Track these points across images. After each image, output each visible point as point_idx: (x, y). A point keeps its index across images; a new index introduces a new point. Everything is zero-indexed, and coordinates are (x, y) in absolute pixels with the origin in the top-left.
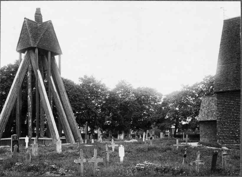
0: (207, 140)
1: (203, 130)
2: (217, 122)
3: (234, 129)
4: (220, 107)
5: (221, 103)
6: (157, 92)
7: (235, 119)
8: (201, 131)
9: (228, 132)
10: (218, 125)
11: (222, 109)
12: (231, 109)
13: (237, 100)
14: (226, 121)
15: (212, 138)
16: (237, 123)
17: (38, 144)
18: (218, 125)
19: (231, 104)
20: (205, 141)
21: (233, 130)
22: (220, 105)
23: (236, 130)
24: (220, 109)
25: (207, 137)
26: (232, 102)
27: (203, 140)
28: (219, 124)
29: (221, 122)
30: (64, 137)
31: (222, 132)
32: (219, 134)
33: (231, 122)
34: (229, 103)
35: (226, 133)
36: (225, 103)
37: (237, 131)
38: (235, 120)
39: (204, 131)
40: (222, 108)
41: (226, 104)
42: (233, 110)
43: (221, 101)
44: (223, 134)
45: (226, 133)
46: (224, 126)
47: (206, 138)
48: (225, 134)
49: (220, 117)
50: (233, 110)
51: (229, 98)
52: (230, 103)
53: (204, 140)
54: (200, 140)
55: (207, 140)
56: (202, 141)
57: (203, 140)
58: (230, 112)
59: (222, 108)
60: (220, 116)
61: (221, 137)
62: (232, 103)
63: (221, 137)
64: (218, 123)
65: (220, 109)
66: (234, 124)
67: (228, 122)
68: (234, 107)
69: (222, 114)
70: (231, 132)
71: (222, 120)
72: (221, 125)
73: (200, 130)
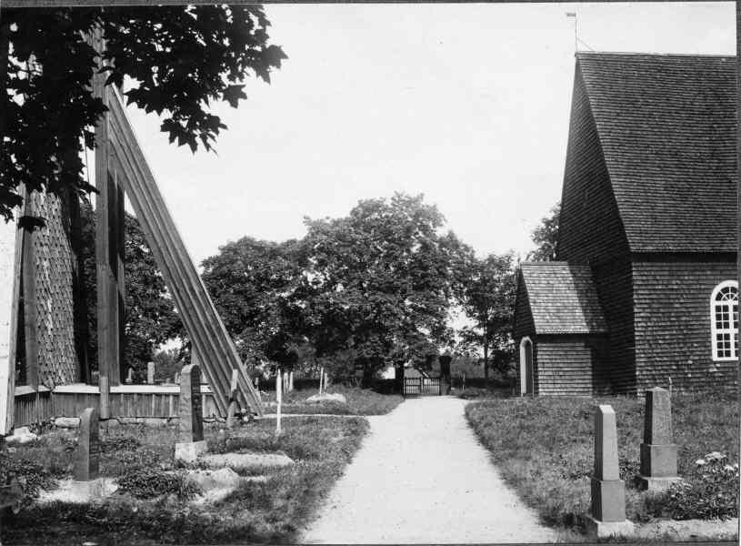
0: (558, 390)
1: (548, 361)
2: (637, 338)
3: (682, 358)
4: (642, 294)
5: (646, 283)
6: (441, 232)
7: (685, 332)
8: (543, 363)
9: (665, 367)
10: (639, 347)
11: (648, 301)
12: (672, 301)
13: (686, 278)
14: (659, 335)
15: (576, 386)
16: (687, 340)
17: (256, 297)
18: (639, 347)
19: (673, 289)
20: (556, 394)
21: (678, 361)
22: (644, 290)
23: (687, 360)
24: (643, 301)
25: (559, 382)
26: (674, 282)
27: (546, 390)
28: (641, 342)
29: (648, 338)
30: (530, 261)
31: (651, 366)
32: (641, 371)
33: (672, 339)
34: (666, 285)
35: (660, 368)
36: (655, 285)
37: (690, 362)
38: (684, 334)
39: (550, 365)
40: (649, 299)
41: (660, 287)
42: (677, 306)
43: (644, 278)
44: (654, 372)
45: (660, 368)
46: (657, 348)
47: (557, 386)
48: (658, 372)
49: (644, 324)
50: (677, 306)
51: (666, 273)
52: (670, 287)
53: (552, 390)
54: (540, 390)
55: (558, 390)
56: (544, 394)
57: (546, 390)
58: (670, 310)
59: (649, 299)
60: (644, 320)
61: (647, 381)
62: (675, 287)
63: (647, 381)
64: (638, 340)
65: (643, 301)
66: (681, 345)
67: (667, 337)
68: (679, 296)
69: (649, 315)
70: (674, 367)
71: (649, 333)
72: (647, 346)
73: (541, 361)
